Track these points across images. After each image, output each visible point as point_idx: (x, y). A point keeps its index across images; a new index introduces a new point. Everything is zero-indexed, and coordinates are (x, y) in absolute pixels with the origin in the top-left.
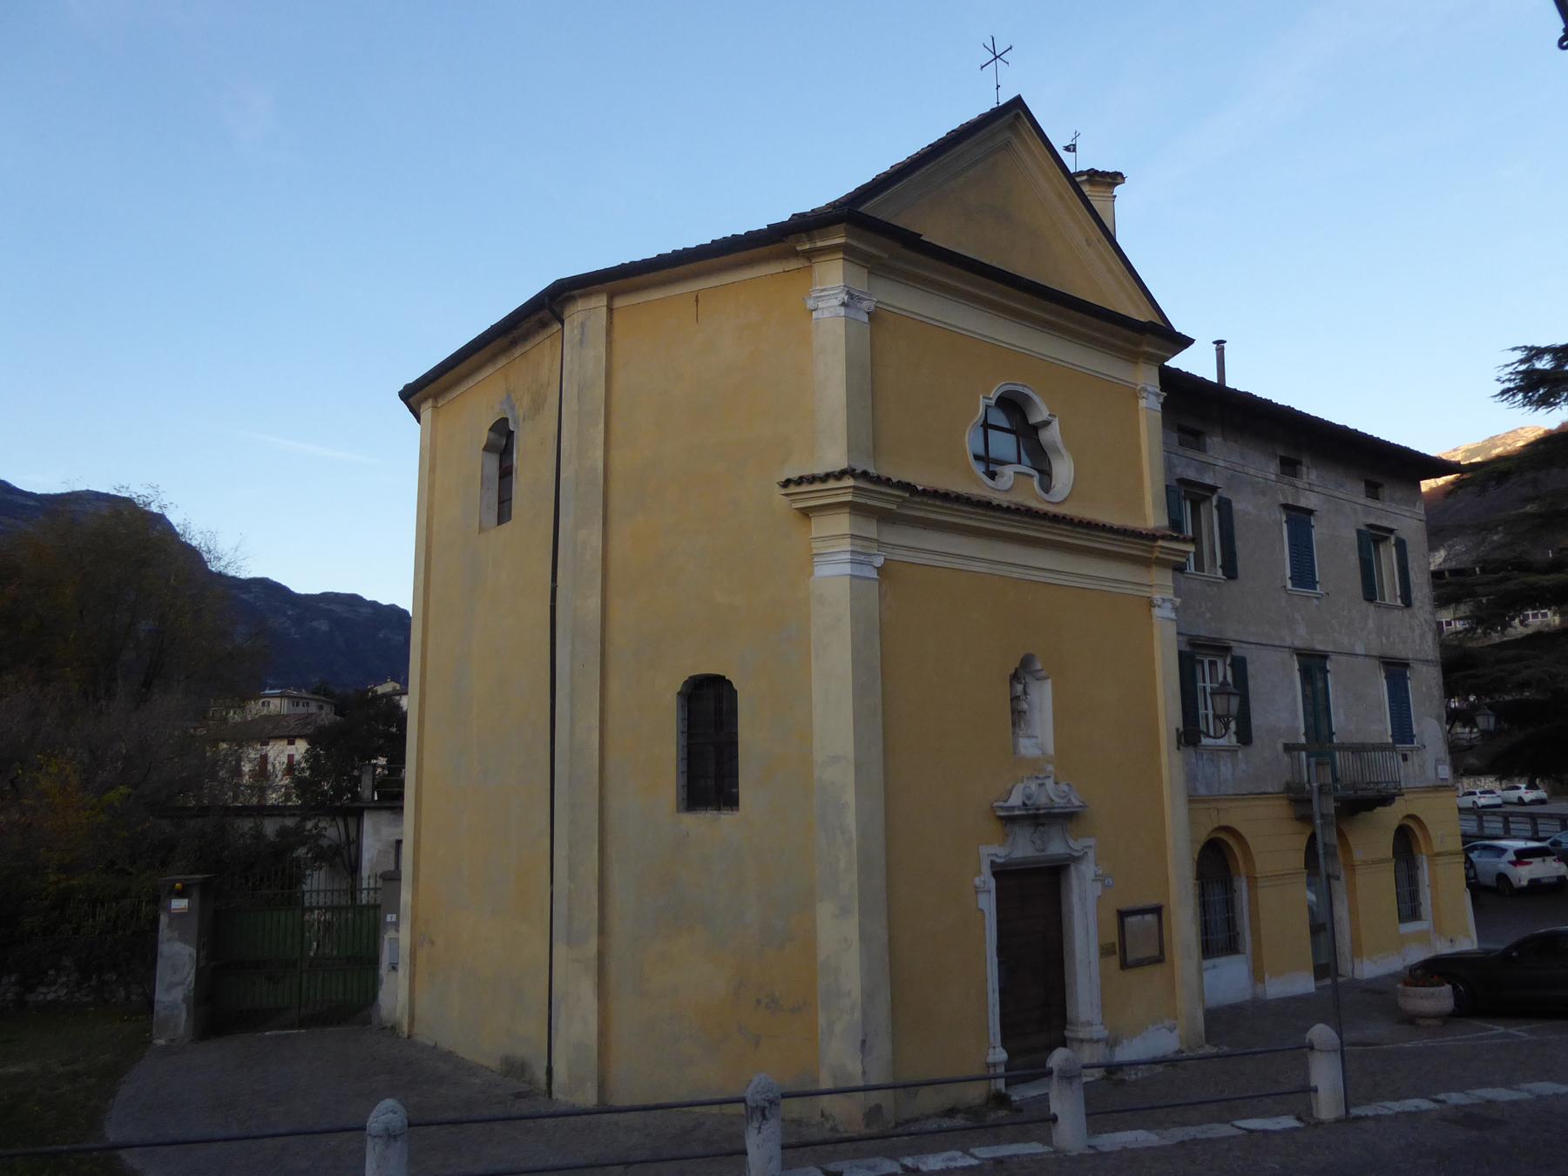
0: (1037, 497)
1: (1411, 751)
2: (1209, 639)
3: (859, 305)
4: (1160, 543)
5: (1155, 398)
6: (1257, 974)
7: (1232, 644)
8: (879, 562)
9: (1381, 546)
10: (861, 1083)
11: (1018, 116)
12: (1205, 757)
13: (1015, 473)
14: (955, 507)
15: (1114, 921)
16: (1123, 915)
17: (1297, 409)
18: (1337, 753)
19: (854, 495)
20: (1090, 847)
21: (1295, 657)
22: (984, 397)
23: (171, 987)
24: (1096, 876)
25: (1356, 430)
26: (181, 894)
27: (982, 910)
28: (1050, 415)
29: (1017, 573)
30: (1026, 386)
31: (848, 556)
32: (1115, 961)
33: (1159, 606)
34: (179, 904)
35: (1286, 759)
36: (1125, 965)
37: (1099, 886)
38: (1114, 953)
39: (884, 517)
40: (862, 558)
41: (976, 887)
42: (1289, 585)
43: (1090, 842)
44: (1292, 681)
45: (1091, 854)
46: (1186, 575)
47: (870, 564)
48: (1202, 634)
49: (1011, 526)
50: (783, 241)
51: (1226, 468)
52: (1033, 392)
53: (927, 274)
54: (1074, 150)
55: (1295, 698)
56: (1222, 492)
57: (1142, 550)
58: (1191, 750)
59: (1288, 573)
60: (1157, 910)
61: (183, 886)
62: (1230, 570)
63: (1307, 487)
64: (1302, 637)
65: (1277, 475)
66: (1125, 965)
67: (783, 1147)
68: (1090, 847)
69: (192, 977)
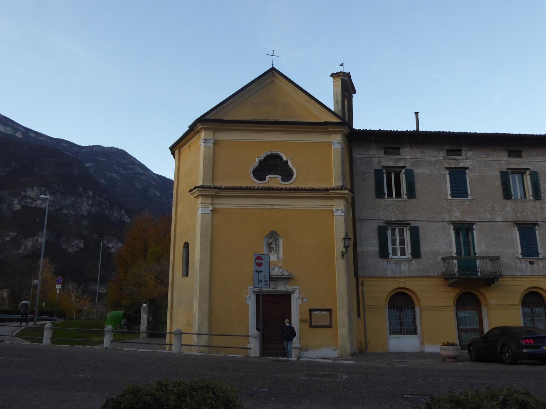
0: (280, 184)
1: (537, 260)
2: (396, 221)
3: (209, 142)
4: (330, 191)
5: (338, 144)
6: (422, 343)
7: (411, 222)
8: (211, 209)
9: (524, 175)
10: (197, 344)
11: (273, 73)
12: (392, 263)
13: (269, 178)
14: (233, 191)
15: (308, 312)
16: (311, 311)
17: (433, 131)
18: (477, 260)
19: (199, 192)
20: (297, 288)
21: (451, 225)
22: (258, 158)
23: (143, 324)
24: (298, 297)
25: (470, 132)
26: (145, 303)
27: (248, 304)
28: (287, 158)
29: (268, 207)
30: (276, 151)
31: (200, 208)
32: (307, 325)
33: (335, 212)
34: (145, 305)
35: (442, 264)
36: (311, 326)
37: (300, 302)
38: (307, 322)
39: (213, 197)
40: (205, 208)
41: (246, 298)
42: (450, 197)
43: (298, 287)
44: (449, 235)
45: (297, 291)
46: (385, 199)
47: (208, 210)
48: (393, 219)
49: (262, 194)
50: (193, 130)
51: (412, 159)
52: (280, 152)
53: (230, 128)
54: (343, 65)
55: (450, 241)
56: (408, 167)
57: (326, 195)
58: (384, 260)
59: (449, 192)
60: (330, 311)
61: (145, 301)
62: (411, 194)
63: (465, 158)
64: (457, 216)
65: (444, 157)
66: (311, 326)
67: (111, 342)
68: (297, 288)
69: (147, 323)
